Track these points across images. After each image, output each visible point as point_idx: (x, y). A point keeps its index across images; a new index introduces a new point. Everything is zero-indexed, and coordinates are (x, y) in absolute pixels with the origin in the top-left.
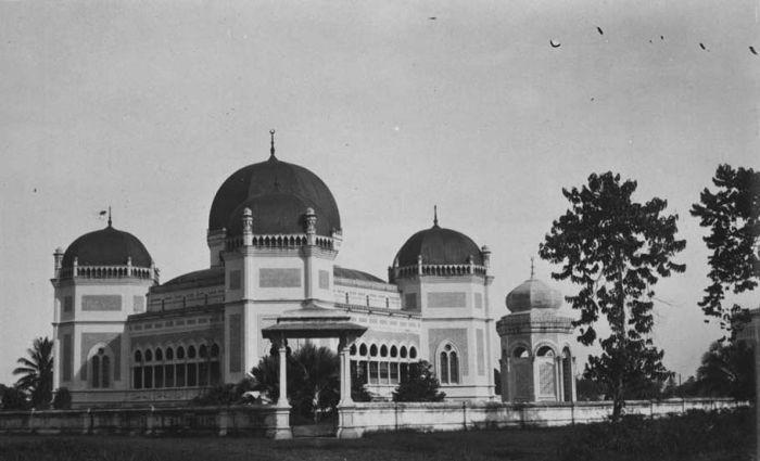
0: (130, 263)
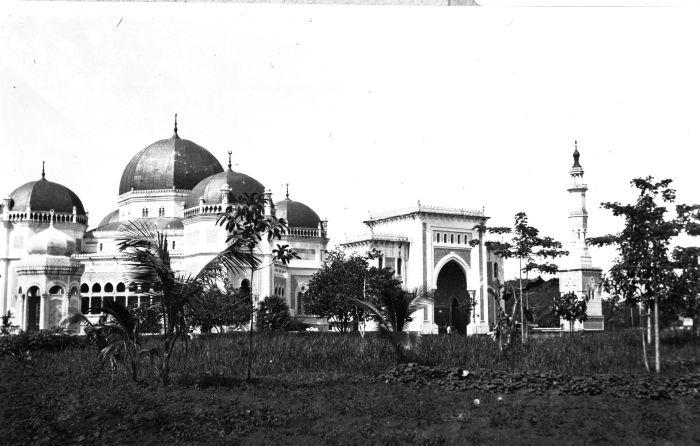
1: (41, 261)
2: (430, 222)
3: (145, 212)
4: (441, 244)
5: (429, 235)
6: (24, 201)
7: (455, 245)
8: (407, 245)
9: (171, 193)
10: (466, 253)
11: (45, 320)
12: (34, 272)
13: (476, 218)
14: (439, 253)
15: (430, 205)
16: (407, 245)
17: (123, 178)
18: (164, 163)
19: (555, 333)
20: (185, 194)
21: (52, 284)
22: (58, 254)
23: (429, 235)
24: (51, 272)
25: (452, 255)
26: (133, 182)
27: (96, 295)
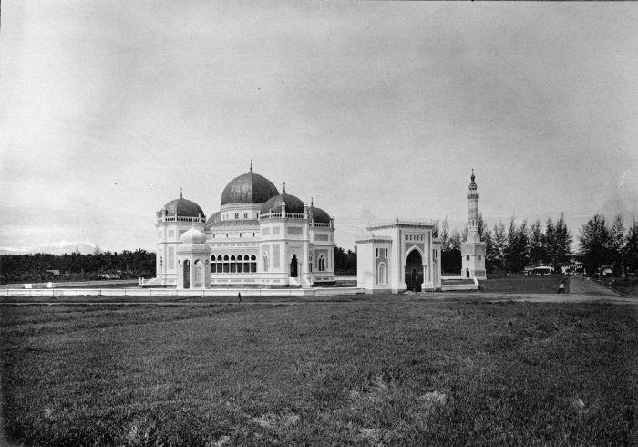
1: (190, 246)
2: (404, 230)
3: (237, 215)
4: (409, 241)
5: (403, 237)
6: (173, 209)
7: (417, 241)
8: (391, 242)
9: (251, 205)
10: (421, 245)
11: (547, 304)
12: (188, 253)
13: (431, 227)
14: (408, 245)
15: (406, 219)
16: (391, 242)
17: (222, 199)
18: (247, 188)
19: (184, 306)
20: (259, 205)
21: (195, 260)
22: (279, 263)
23: (403, 237)
24: (195, 253)
25: (414, 247)
26: (227, 199)
27: (233, 262)
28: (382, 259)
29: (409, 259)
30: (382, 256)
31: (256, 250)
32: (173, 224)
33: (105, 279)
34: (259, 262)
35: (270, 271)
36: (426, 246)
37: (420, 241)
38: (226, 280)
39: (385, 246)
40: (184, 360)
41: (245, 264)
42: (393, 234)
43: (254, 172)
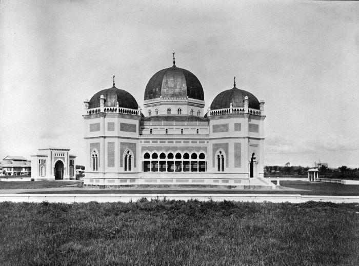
0: (231, 106)
2: (53, 151)
3: (169, 110)
4: (56, 156)
28: (42, 164)
29: (56, 165)
30: (42, 163)
31: (205, 149)
32: (113, 116)
33: (316, 177)
34: (208, 159)
35: (100, 170)
36: (66, 159)
37: (62, 156)
38: (187, 179)
39: (44, 158)
40: (18, 215)
41: (177, 162)
42: (48, 153)
43: (177, 66)
